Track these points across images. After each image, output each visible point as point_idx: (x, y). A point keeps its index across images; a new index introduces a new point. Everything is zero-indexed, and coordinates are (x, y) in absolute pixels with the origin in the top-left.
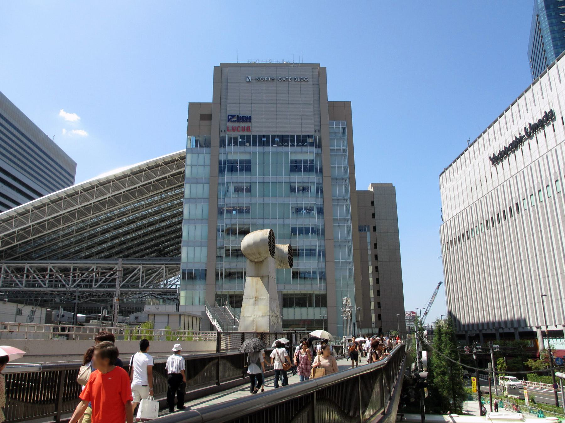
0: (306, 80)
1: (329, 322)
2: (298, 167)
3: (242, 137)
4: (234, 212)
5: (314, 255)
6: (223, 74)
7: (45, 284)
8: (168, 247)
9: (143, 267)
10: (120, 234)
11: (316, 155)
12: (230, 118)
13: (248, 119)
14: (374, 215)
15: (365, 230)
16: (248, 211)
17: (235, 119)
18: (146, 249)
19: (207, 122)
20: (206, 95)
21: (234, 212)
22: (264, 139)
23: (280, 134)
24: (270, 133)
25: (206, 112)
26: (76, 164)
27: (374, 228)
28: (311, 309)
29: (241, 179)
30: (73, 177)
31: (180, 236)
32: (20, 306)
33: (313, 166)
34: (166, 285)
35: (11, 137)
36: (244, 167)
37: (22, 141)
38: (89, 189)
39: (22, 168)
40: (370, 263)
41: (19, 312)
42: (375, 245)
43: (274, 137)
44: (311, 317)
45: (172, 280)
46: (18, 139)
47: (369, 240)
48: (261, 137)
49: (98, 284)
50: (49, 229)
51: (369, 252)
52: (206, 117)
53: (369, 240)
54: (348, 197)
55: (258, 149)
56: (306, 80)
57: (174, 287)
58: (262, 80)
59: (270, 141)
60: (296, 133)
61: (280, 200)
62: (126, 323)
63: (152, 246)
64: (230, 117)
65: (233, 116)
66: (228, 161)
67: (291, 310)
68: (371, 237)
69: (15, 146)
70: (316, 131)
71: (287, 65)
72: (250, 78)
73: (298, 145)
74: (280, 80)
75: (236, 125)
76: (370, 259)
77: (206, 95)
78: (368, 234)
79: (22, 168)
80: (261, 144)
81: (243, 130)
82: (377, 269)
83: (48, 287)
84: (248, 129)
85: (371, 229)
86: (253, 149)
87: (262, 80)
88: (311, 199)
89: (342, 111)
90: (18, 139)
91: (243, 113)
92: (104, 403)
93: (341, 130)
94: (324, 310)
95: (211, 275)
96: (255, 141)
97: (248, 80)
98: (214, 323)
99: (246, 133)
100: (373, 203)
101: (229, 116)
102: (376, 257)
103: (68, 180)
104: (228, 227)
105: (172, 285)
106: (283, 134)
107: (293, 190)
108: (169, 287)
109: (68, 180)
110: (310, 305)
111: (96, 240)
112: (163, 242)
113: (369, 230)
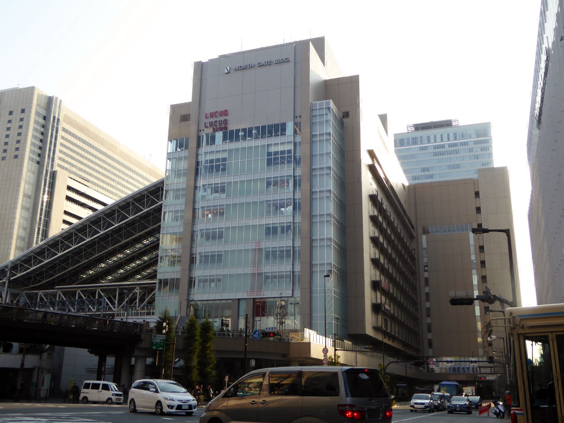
0: (287, 61)
2: (273, 160)
5: (282, 257)
11: (295, 144)
14: (478, 210)
20: (185, 95)
21: (210, 216)
23: (256, 125)
24: (246, 126)
25: (184, 113)
29: (217, 179)
31: (155, 246)
36: (217, 167)
40: (474, 271)
43: (250, 130)
48: (238, 131)
49: (116, 302)
51: (473, 257)
52: (185, 118)
59: (248, 133)
61: (257, 199)
62: (498, 408)
74: (261, 65)
77: (185, 95)
80: (237, 139)
82: (483, 279)
88: (287, 193)
92: (111, 414)
100: (477, 194)
102: (483, 263)
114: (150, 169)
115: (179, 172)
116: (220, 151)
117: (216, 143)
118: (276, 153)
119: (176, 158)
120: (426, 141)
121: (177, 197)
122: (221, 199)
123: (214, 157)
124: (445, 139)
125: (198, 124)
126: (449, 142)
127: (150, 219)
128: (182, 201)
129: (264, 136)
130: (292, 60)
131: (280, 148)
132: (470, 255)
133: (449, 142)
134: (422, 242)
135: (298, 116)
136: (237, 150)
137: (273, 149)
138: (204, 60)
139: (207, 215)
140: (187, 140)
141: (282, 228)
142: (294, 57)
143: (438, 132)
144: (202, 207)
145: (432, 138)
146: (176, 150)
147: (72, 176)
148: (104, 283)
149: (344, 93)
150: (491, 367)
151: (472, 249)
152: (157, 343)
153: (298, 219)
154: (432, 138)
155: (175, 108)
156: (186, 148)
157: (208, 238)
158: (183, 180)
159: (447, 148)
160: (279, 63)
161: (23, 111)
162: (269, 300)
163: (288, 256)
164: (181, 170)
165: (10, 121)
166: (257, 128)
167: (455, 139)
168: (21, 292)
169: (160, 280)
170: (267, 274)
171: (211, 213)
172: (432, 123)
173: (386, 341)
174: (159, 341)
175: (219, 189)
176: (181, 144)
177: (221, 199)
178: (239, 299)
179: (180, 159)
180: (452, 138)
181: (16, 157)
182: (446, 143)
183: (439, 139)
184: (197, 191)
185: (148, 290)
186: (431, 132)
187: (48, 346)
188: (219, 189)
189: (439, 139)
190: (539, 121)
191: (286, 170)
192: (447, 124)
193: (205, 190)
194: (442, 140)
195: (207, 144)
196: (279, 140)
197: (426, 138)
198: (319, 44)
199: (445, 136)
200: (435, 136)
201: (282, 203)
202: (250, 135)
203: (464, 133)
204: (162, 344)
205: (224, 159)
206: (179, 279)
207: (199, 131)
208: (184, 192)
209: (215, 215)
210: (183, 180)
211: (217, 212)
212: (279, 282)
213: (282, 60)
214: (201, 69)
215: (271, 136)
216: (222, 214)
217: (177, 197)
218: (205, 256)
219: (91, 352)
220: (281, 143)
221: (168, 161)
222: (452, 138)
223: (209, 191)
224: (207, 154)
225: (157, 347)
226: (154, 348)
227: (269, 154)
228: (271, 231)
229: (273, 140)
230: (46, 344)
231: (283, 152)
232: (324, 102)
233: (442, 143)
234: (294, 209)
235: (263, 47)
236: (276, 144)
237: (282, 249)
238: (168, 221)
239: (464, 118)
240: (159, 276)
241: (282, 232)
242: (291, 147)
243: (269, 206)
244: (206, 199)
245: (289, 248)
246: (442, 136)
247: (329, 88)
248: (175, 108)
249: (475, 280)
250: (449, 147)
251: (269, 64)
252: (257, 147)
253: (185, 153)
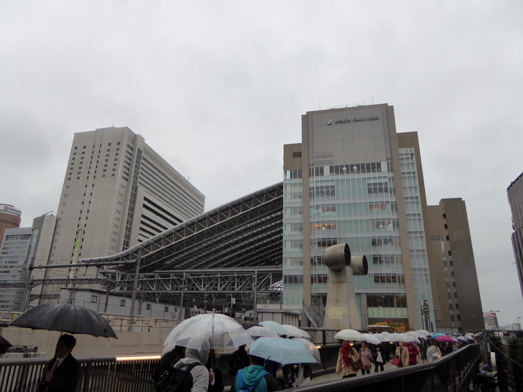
1: (410, 320)
2: (373, 189)
4: (324, 228)
6: (309, 120)
7: (153, 288)
8: (273, 257)
10: (237, 248)
15: (439, 240)
16: (334, 227)
18: (257, 259)
19: (298, 159)
20: (296, 137)
22: (345, 168)
25: (298, 151)
26: (205, 197)
28: (392, 309)
30: (203, 207)
32: (167, 306)
33: (387, 187)
34: (272, 288)
35: (196, 208)
37: (167, 183)
38: (215, 214)
39: (168, 202)
41: (166, 310)
43: (352, 166)
44: (393, 316)
45: (277, 284)
46: (153, 172)
48: (342, 167)
50: (187, 247)
52: (298, 155)
54: (420, 211)
55: (340, 177)
56: (377, 119)
57: (279, 289)
58: (341, 122)
63: (261, 257)
66: (316, 187)
67: (375, 309)
69: (149, 177)
71: (360, 108)
72: (330, 121)
73: (373, 171)
77: (296, 137)
78: (442, 243)
79: (168, 202)
80: (342, 172)
83: (171, 290)
87: (341, 122)
89: (411, 139)
90: (172, 187)
93: (410, 156)
94: (404, 309)
95: (307, 280)
97: (329, 123)
98: (310, 320)
103: (200, 209)
104: (319, 240)
105: (278, 288)
106: (360, 163)
108: (275, 289)
109: (200, 209)
110: (392, 306)
111: (220, 254)
112: (270, 254)
113: (442, 240)
117: (325, 174)
142: (303, 116)
147: (147, 190)
155: (287, 148)
156: (300, 176)
158: (298, 200)
161: (119, 143)
165: (109, 150)
166: (358, 166)
168: (127, 274)
181: (113, 175)
191: (387, 198)
193: (317, 209)
196: (377, 174)
205: (333, 187)
206: (302, 276)
220: (379, 177)
227: (369, 185)
229: (372, 175)
232: (409, 149)
248: (287, 148)
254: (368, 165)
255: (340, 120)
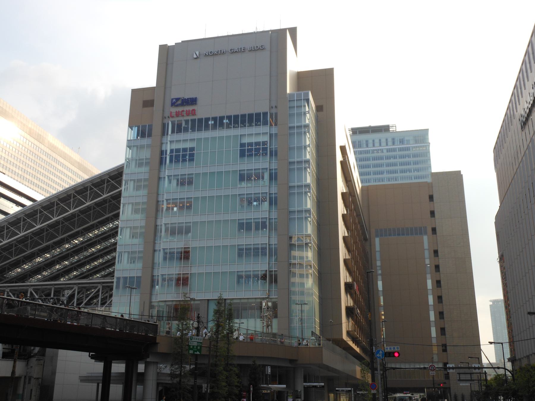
0: (262, 48)
2: (247, 151)
3: (187, 122)
6: (166, 54)
9: (103, 287)
11: (271, 135)
12: (174, 103)
13: (193, 101)
14: (432, 213)
15: (421, 233)
17: (179, 102)
20: (149, 80)
21: (175, 209)
23: (229, 114)
25: (149, 98)
27: (434, 230)
29: (184, 169)
36: (184, 156)
40: (428, 276)
42: (436, 252)
43: (222, 118)
47: (426, 246)
48: (207, 120)
51: (427, 261)
52: (148, 104)
53: (426, 246)
55: (203, 134)
60: (247, 110)
64: (174, 100)
65: (177, 99)
68: (429, 243)
70: (276, 107)
74: (233, 52)
75: (180, 109)
76: (428, 270)
77: (149, 80)
78: (425, 238)
80: (207, 127)
81: (188, 115)
84: (193, 112)
85: (430, 231)
86: (196, 135)
88: (262, 187)
91: (188, 95)
96: (201, 124)
97: (195, 56)
99: (190, 118)
100: (431, 198)
101: (172, 99)
102: (437, 267)
107: (242, 178)
113: (426, 233)
114: (79, 163)
115: (141, 161)
116: (187, 140)
118: (250, 144)
119: (137, 147)
120: (365, 145)
121: (138, 188)
122: (186, 193)
123: (181, 146)
124: (384, 144)
125: (163, 111)
126: (387, 147)
127: (75, 221)
128: (143, 192)
129: (259, 123)
130: (268, 47)
131: (253, 140)
132: (376, 260)
133: (387, 147)
134: (375, 245)
135: (274, 106)
136: (206, 139)
137: (246, 140)
138: (171, 43)
139: (173, 209)
140: (150, 127)
141: (257, 224)
142: (274, 44)
143: (376, 136)
144: (167, 200)
145: (370, 142)
146: (137, 138)
148: (34, 281)
149: (320, 84)
150: (471, 374)
151: (427, 254)
152: (193, 346)
153: (274, 215)
154: (370, 142)
156: (150, 135)
157: (173, 233)
158: (145, 169)
159: (385, 154)
160: (254, 50)
162: (235, 301)
163: (263, 254)
164: (143, 159)
166: (229, 118)
167: (394, 143)
169: (118, 278)
170: (239, 274)
171: (176, 206)
172: (370, 127)
173: (351, 343)
174: (195, 344)
175: (185, 182)
176: (143, 133)
177: (186, 193)
178: (208, 300)
179: (142, 147)
180: (390, 143)
182: (384, 147)
183: (377, 144)
184: (161, 183)
185: (108, 289)
186: (370, 137)
187: (37, 349)
188: (185, 182)
189: (377, 144)
190: (524, 123)
192: (385, 129)
194: (380, 145)
195: (173, 132)
197: (364, 142)
198: (293, 31)
199: (383, 141)
200: (373, 141)
201: (249, 198)
202: (222, 125)
203: (403, 138)
204: (199, 348)
205: (192, 149)
207: (164, 118)
208: (146, 183)
209: (181, 208)
210: (145, 169)
211: (183, 206)
212: (168, 286)
213: (257, 47)
214: (166, 54)
215: (245, 126)
216: (189, 208)
217: (138, 188)
218: (170, 253)
219: (92, 357)
220: (256, 134)
221: (128, 149)
222: (390, 143)
223: (174, 182)
224: (172, 142)
225: (194, 351)
226: (191, 352)
227: (242, 145)
228: (245, 226)
229: (246, 130)
230: (35, 346)
231: (257, 144)
233: (380, 148)
234: (271, 204)
235: (229, 34)
236: (250, 135)
237: (172, 251)
238: (126, 212)
239: (402, 124)
240: (116, 274)
241: (257, 229)
242: (266, 138)
243: (242, 200)
244: (169, 189)
245: (264, 246)
246: (380, 140)
247: (305, 79)
249: (429, 284)
250: (387, 151)
251: (242, 51)
252: (228, 137)
253: (146, 141)
254: (243, 116)
255: (211, 52)
